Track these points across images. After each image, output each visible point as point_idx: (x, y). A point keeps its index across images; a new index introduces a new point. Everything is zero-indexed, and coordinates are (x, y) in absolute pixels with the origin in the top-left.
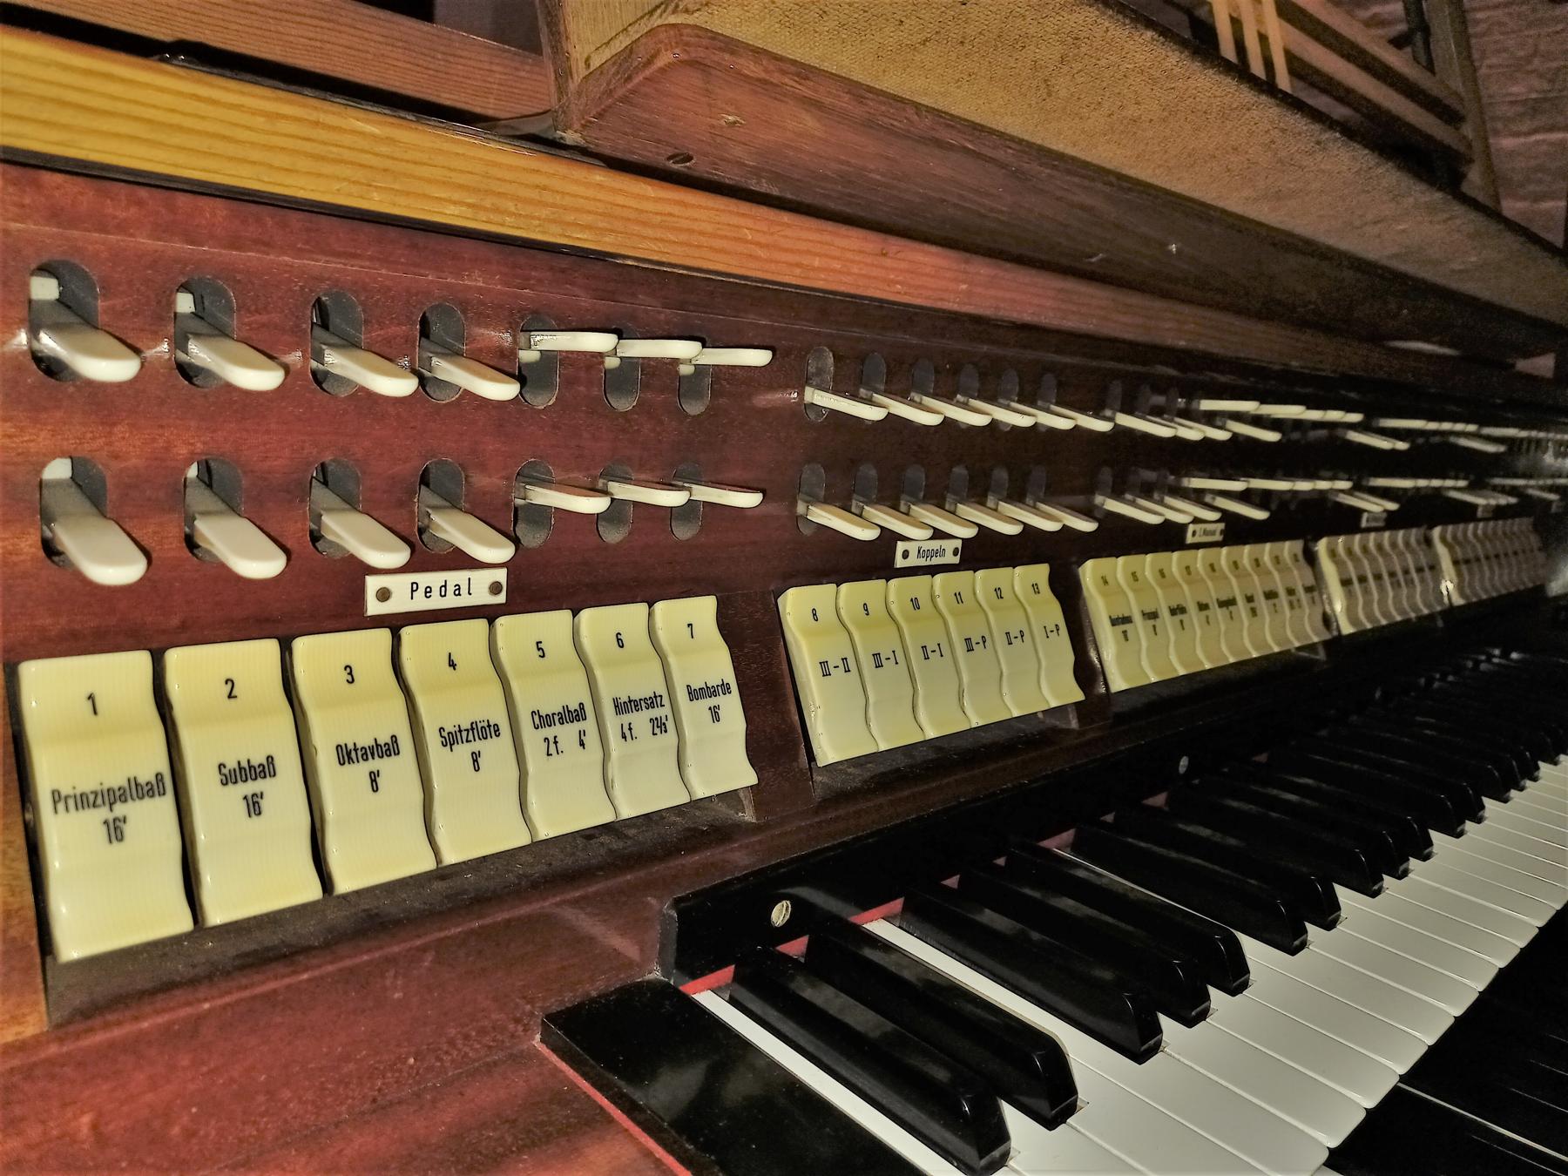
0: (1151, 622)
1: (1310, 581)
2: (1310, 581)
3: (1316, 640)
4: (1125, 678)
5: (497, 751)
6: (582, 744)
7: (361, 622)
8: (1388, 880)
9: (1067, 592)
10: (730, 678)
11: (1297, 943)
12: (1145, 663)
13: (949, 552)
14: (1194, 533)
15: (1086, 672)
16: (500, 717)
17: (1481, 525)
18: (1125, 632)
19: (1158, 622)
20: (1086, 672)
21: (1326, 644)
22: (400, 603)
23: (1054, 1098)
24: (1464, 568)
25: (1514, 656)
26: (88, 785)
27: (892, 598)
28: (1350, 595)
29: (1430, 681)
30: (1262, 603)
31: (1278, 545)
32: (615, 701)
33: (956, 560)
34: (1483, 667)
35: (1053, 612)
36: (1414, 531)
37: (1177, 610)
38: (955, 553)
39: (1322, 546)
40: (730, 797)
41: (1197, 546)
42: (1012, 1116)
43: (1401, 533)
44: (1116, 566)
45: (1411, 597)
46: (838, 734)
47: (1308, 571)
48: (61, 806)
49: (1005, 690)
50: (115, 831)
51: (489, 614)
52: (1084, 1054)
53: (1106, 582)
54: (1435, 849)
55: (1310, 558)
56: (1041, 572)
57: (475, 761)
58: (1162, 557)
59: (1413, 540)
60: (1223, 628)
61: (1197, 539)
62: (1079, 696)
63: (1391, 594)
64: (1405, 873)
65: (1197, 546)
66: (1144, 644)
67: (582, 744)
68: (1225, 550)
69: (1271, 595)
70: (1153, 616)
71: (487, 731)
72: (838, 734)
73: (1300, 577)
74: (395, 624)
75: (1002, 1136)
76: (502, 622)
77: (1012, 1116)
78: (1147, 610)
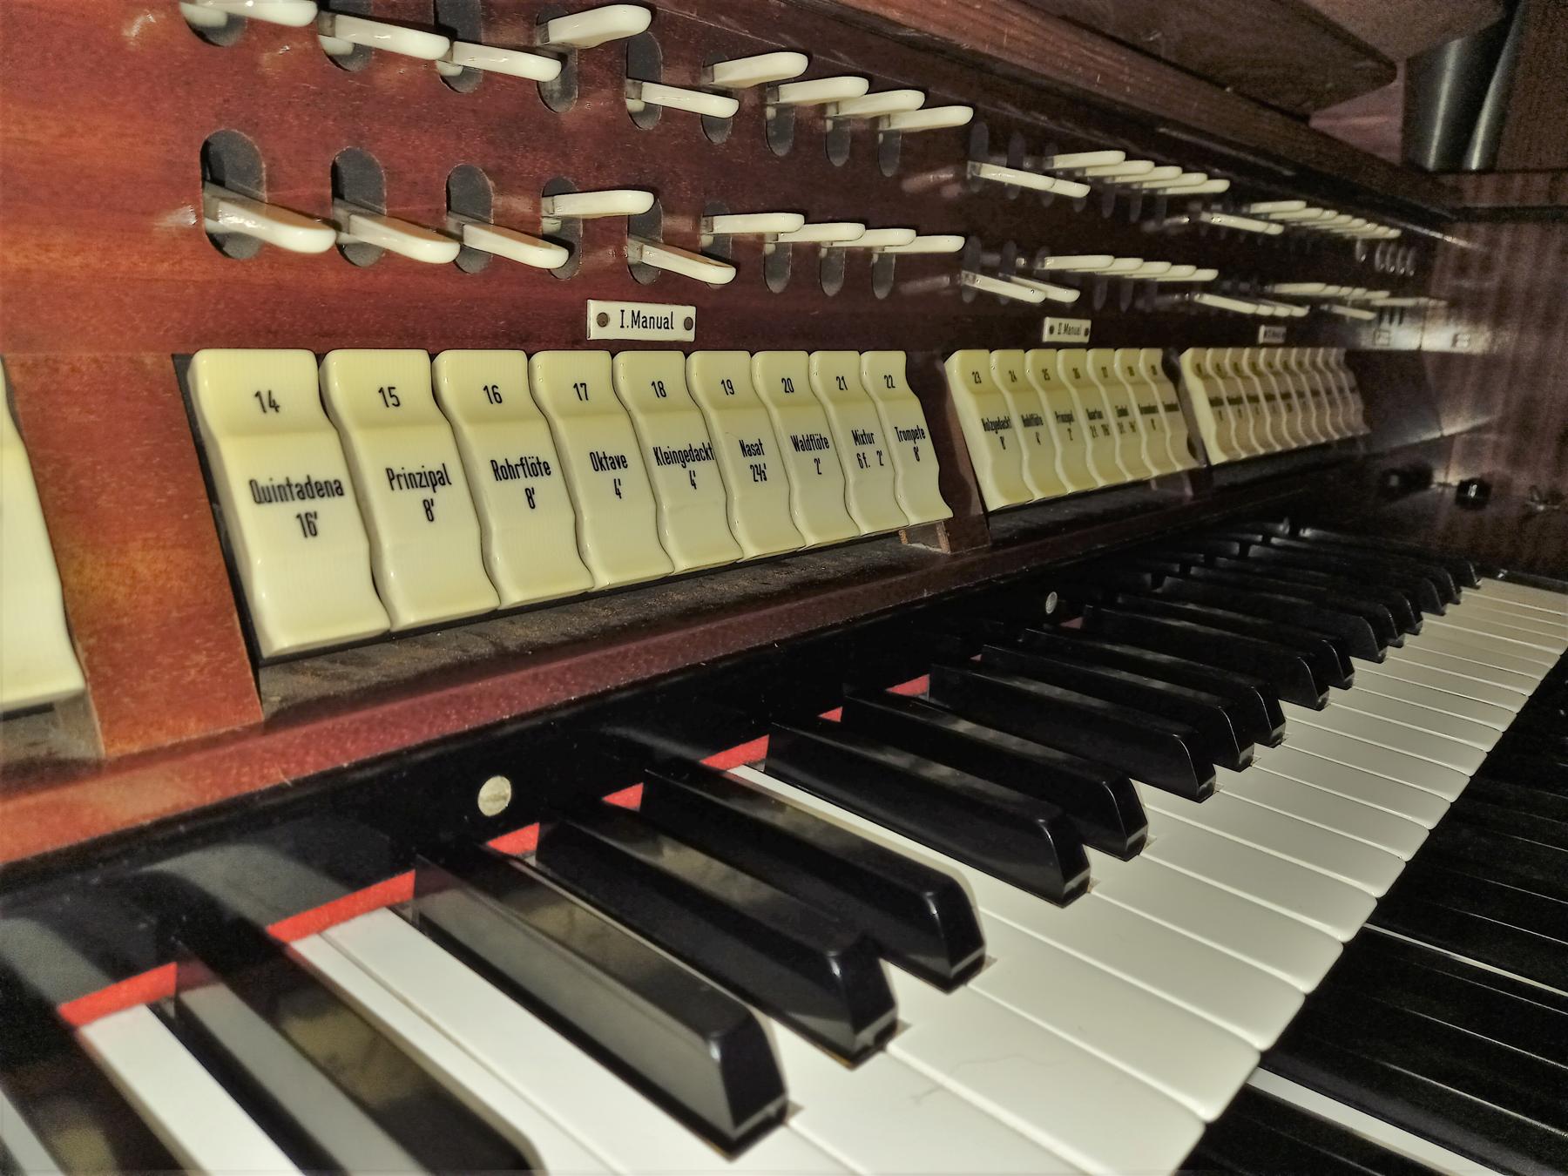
0: (1067, 425)
1: (1173, 399)
2: (1173, 399)
3: (1179, 468)
4: (1005, 493)
5: (335, 513)
6: (618, 493)
7: (577, 340)
8: (1222, 774)
9: (928, 387)
10: (924, 426)
11: (1072, 884)
12: (1119, 461)
13: (678, 323)
14: (1051, 330)
15: (956, 481)
16: (341, 474)
17: (1263, 352)
18: (817, 461)
19: (1073, 426)
20: (956, 481)
21: (1192, 474)
22: (612, 332)
23: (953, 949)
24: (1229, 410)
25: (1308, 533)
26: (413, 467)
27: (865, 369)
28: (1220, 417)
29: (1245, 546)
30: (1295, 400)
31: (1220, 351)
32: (252, 483)
33: (690, 336)
34: (1254, 551)
35: (913, 414)
36: (1334, 351)
37: (1031, 421)
38: (688, 324)
39: (1187, 359)
40: (926, 531)
41: (1058, 346)
42: (899, 980)
43: (1294, 351)
44: (1241, 356)
45: (1306, 423)
46: (303, 593)
47: (1169, 386)
48: (395, 482)
49: (668, 533)
50: (309, 525)
51: (686, 349)
52: (993, 900)
53: (1014, 379)
54: (1152, 831)
55: (1173, 373)
56: (895, 361)
57: (530, 498)
58: (1015, 354)
59: (1332, 360)
60: (1168, 435)
61: (1055, 338)
62: (946, 513)
63: (1269, 420)
64: (1248, 763)
65: (1058, 346)
66: (1026, 457)
67: (618, 493)
68: (1092, 353)
69: (1286, 396)
70: (1067, 418)
71: (538, 468)
72: (303, 593)
73: (1160, 393)
74: (614, 347)
75: (885, 1001)
76: (696, 357)
77: (899, 980)
78: (1062, 412)
